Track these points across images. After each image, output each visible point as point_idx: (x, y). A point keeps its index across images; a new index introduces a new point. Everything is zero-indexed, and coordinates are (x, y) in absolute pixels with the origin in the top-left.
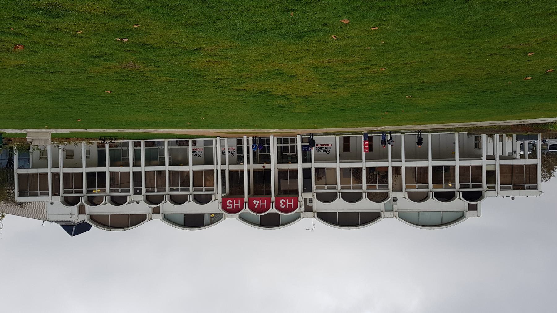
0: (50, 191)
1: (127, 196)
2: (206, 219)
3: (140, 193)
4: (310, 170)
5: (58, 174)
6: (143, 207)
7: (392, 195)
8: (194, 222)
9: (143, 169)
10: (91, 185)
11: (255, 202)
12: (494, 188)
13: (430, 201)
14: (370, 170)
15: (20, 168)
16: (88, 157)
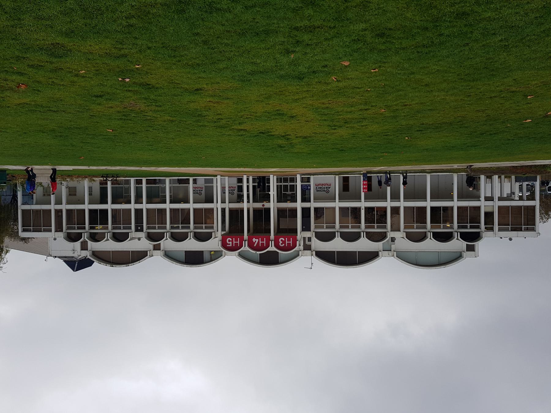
0: (53, 228)
1: (211, 233)
2: (206, 256)
3: (142, 230)
4: (309, 209)
5: (61, 211)
6: (144, 244)
7: (391, 235)
8: (194, 259)
9: (144, 206)
10: (93, 221)
11: (254, 240)
12: (492, 229)
13: (427, 241)
14: (369, 210)
15: (23, 204)
16: (90, 194)
